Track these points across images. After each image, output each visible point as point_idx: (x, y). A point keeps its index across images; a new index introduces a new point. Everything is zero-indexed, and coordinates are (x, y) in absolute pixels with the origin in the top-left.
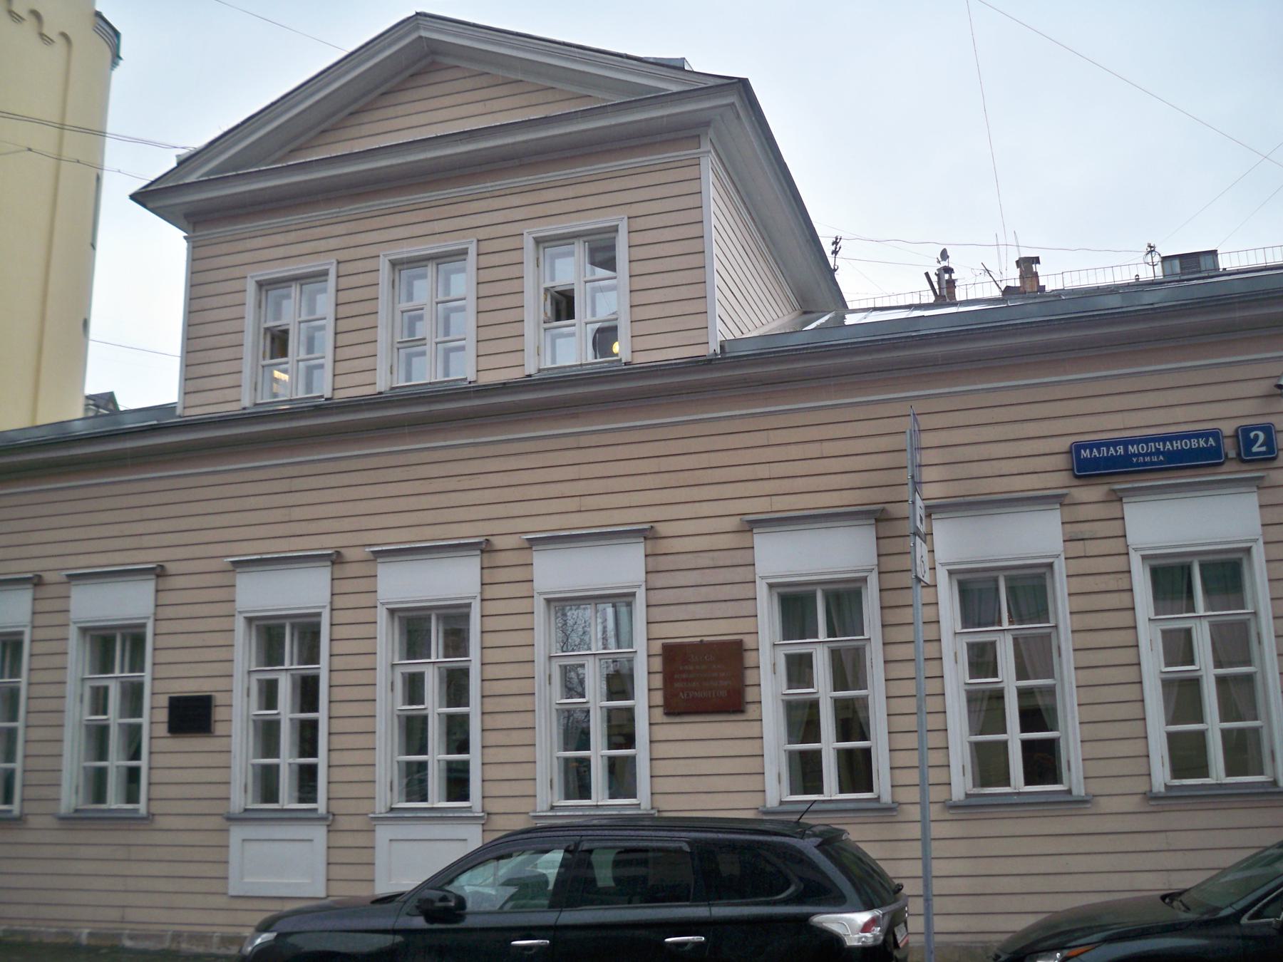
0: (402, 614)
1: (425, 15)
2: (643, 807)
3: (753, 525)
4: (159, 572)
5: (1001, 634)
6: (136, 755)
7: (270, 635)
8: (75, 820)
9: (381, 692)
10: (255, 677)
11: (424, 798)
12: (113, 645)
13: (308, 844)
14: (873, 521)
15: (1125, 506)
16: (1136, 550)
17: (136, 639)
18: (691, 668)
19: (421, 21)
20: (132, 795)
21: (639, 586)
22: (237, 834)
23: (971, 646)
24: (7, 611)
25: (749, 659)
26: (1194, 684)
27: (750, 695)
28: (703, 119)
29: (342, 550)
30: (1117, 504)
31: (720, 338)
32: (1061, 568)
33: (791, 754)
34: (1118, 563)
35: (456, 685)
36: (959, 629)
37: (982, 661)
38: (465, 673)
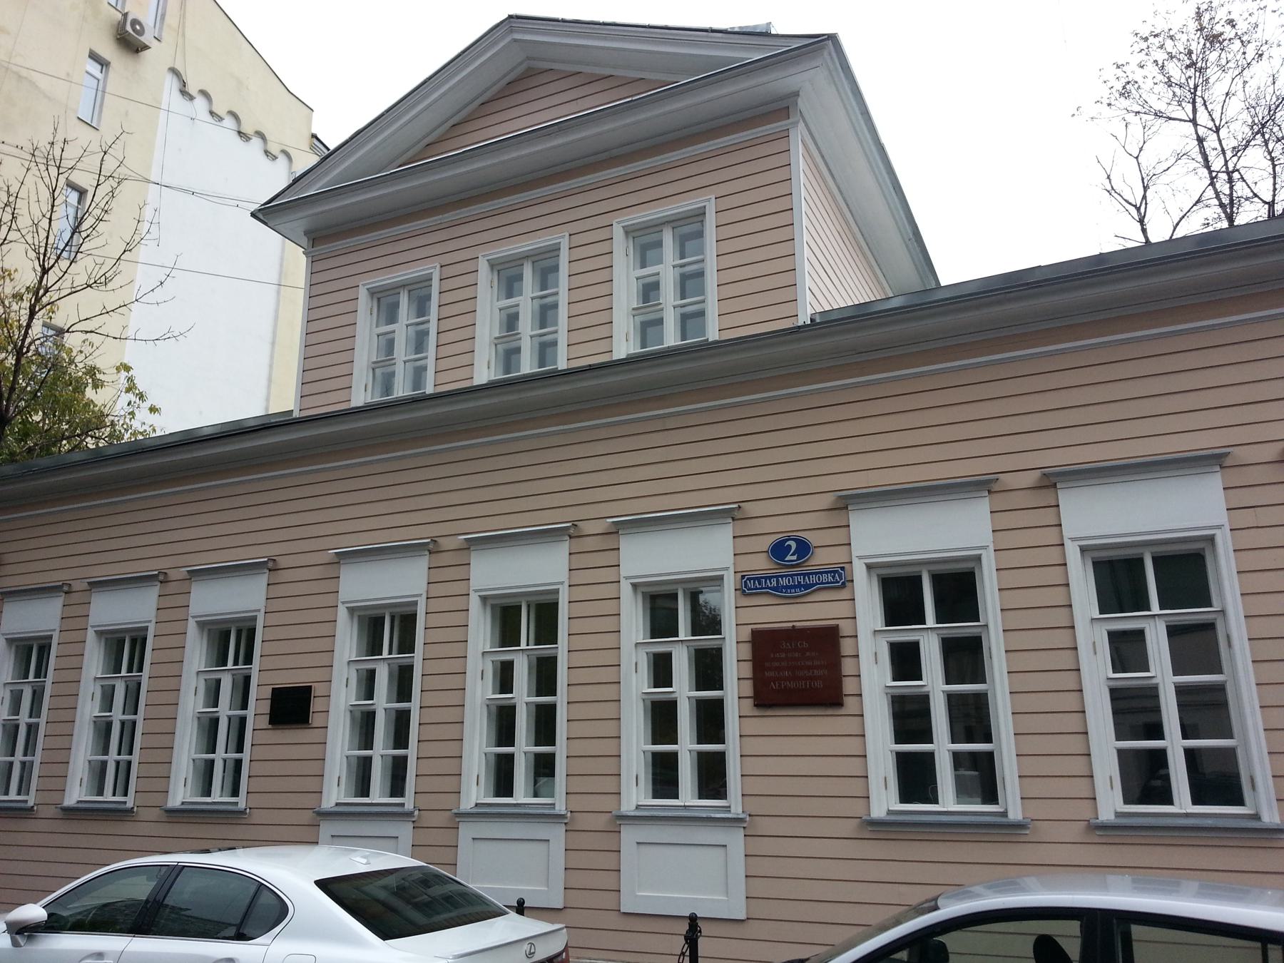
0: (362, 613)
1: (518, 17)
2: (733, 809)
4: (271, 566)
5: (1151, 621)
6: (240, 749)
8: (481, 814)
10: (489, 659)
11: (509, 793)
12: (233, 639)
13: (393, 841)
16: (476, 591)
17: (407, 621)
18: (783, 655)
19: (516, 24)
20: (397, 787)
25: (846, 647)
27: (848, 686)
28: (758, 99)
30: (1050, 492)
31: (810, 311)
32: (1225, 544)
33: (1121, 752)
34: (1052, 556)
35: (545, 676)
36: (1097, 615)
37: (1127, 649)
38: (553, 660)
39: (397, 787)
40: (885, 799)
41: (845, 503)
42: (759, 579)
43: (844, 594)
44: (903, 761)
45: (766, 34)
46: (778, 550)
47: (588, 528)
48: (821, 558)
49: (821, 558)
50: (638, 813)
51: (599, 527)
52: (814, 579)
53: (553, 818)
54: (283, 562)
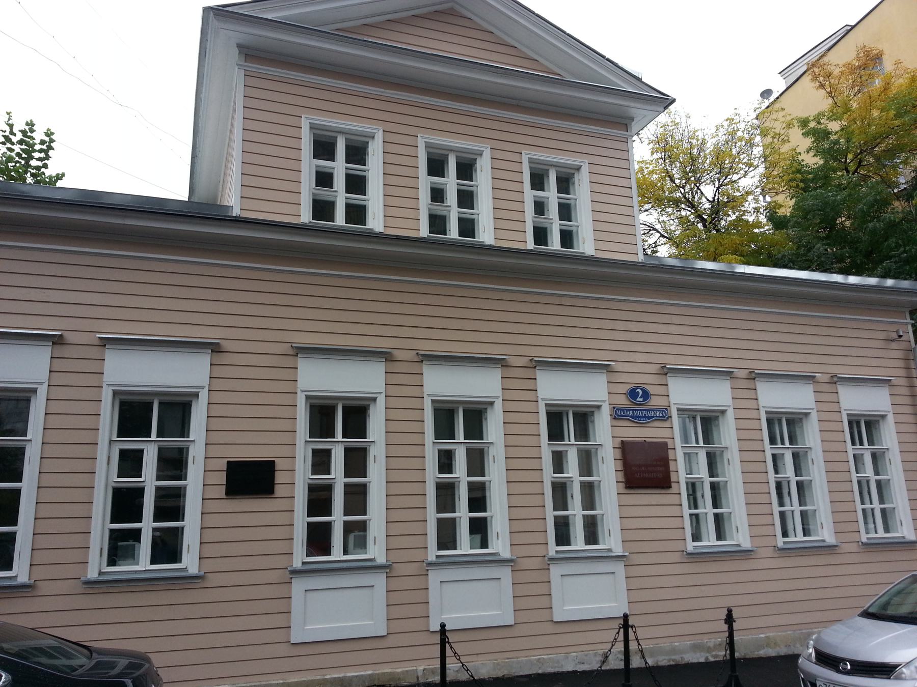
3: (105, 343)
4: (57, 341)
7: (322, 415)
9: (101, 465)
14: (51, 344)
15: (669, 379)
20: (592, 537)
21: (41, 383)
22: (298, 586)
23: (314, 452)
24: (25, 367)
26: (328, 488)
29: (65, 333)
39: (592, 537)
40: (96, 565)
41: (665, 371)
42: (623, 410)
43: (667, 424)
44: (312, 528)
45: (639, 80)
46: (633, 394)
47: (513, 361)
48: (655, 402)
49: (655, 402)
50: (101, 578)
51: (410, 355)
52: (652, 414)
53: (370, 567)
54: (70, 337)
